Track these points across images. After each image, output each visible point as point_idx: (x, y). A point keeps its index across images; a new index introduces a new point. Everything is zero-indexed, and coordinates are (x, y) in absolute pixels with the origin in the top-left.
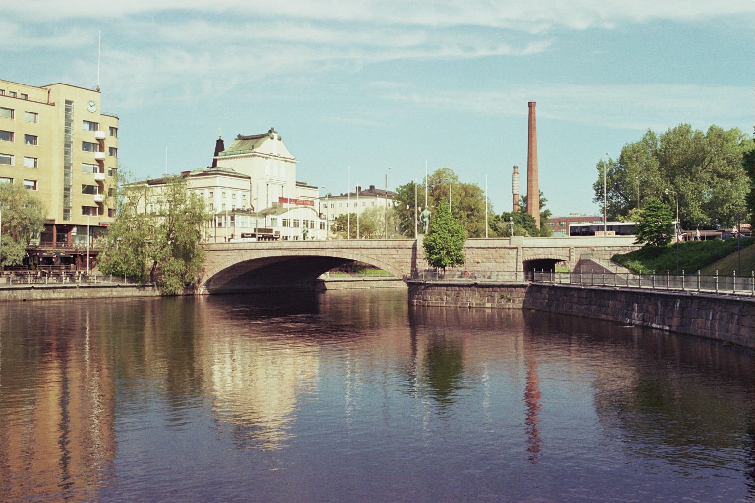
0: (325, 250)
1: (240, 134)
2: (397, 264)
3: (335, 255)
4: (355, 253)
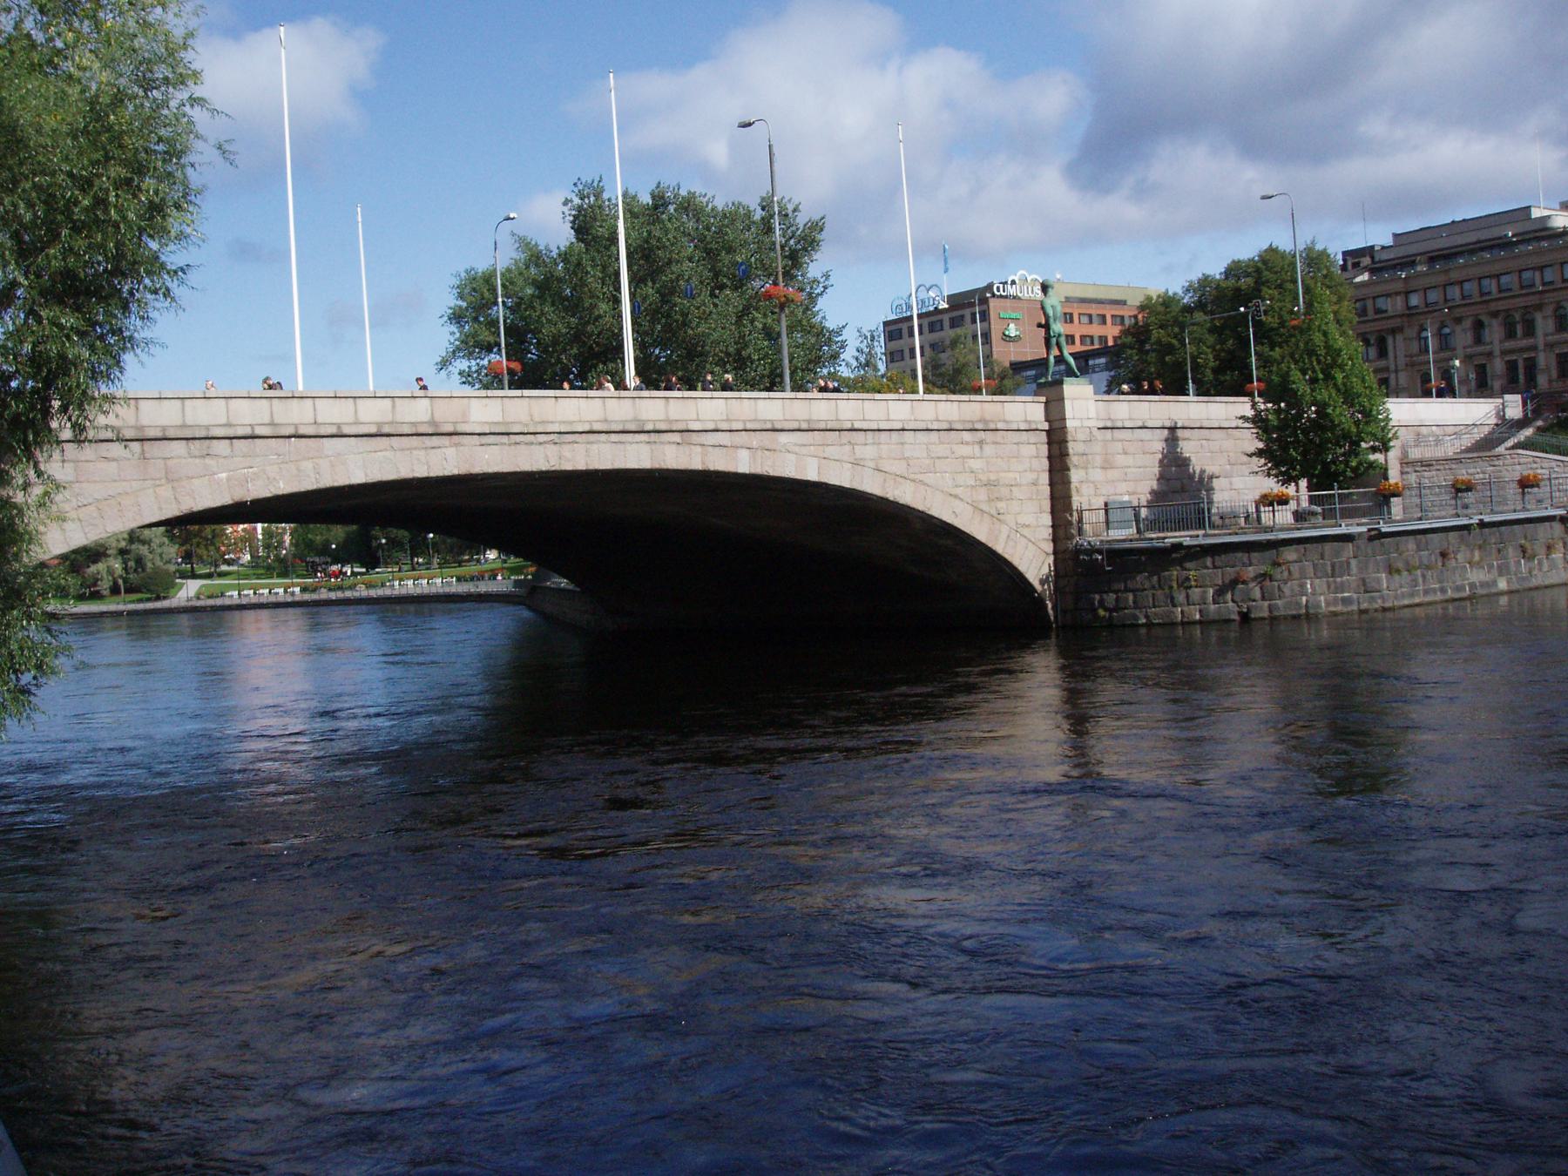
0: (695, 437)
1: (808, 241)
3: (743, 463)
4: (831, 451)
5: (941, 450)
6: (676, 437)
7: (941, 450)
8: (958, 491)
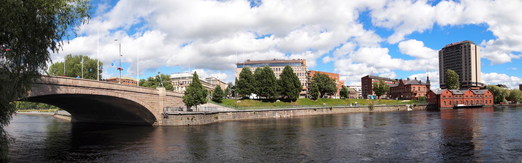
2: (151, 104)
5: (146, 96)
6: (110, 90)
7: (146, 96)
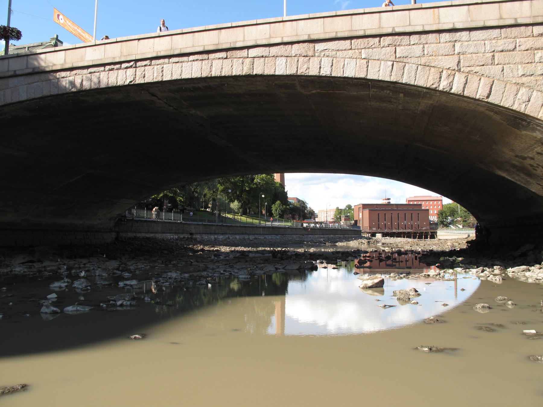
0: (244, 53)
5: (501, 44)
8: (524, 80)
